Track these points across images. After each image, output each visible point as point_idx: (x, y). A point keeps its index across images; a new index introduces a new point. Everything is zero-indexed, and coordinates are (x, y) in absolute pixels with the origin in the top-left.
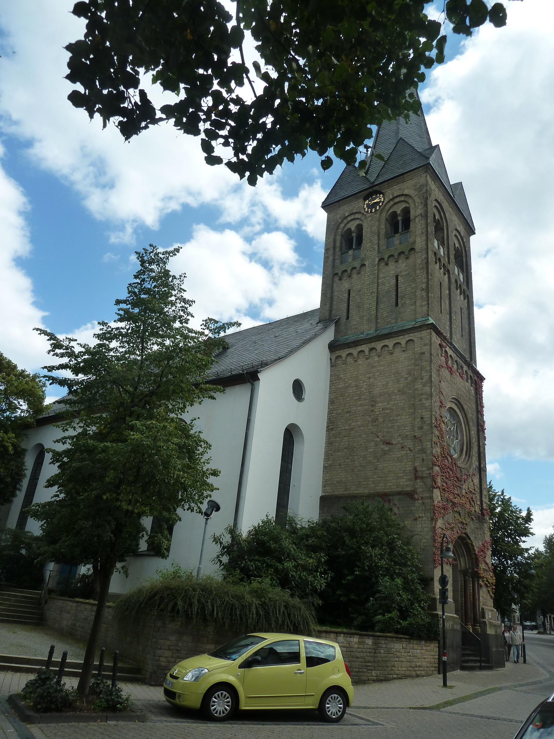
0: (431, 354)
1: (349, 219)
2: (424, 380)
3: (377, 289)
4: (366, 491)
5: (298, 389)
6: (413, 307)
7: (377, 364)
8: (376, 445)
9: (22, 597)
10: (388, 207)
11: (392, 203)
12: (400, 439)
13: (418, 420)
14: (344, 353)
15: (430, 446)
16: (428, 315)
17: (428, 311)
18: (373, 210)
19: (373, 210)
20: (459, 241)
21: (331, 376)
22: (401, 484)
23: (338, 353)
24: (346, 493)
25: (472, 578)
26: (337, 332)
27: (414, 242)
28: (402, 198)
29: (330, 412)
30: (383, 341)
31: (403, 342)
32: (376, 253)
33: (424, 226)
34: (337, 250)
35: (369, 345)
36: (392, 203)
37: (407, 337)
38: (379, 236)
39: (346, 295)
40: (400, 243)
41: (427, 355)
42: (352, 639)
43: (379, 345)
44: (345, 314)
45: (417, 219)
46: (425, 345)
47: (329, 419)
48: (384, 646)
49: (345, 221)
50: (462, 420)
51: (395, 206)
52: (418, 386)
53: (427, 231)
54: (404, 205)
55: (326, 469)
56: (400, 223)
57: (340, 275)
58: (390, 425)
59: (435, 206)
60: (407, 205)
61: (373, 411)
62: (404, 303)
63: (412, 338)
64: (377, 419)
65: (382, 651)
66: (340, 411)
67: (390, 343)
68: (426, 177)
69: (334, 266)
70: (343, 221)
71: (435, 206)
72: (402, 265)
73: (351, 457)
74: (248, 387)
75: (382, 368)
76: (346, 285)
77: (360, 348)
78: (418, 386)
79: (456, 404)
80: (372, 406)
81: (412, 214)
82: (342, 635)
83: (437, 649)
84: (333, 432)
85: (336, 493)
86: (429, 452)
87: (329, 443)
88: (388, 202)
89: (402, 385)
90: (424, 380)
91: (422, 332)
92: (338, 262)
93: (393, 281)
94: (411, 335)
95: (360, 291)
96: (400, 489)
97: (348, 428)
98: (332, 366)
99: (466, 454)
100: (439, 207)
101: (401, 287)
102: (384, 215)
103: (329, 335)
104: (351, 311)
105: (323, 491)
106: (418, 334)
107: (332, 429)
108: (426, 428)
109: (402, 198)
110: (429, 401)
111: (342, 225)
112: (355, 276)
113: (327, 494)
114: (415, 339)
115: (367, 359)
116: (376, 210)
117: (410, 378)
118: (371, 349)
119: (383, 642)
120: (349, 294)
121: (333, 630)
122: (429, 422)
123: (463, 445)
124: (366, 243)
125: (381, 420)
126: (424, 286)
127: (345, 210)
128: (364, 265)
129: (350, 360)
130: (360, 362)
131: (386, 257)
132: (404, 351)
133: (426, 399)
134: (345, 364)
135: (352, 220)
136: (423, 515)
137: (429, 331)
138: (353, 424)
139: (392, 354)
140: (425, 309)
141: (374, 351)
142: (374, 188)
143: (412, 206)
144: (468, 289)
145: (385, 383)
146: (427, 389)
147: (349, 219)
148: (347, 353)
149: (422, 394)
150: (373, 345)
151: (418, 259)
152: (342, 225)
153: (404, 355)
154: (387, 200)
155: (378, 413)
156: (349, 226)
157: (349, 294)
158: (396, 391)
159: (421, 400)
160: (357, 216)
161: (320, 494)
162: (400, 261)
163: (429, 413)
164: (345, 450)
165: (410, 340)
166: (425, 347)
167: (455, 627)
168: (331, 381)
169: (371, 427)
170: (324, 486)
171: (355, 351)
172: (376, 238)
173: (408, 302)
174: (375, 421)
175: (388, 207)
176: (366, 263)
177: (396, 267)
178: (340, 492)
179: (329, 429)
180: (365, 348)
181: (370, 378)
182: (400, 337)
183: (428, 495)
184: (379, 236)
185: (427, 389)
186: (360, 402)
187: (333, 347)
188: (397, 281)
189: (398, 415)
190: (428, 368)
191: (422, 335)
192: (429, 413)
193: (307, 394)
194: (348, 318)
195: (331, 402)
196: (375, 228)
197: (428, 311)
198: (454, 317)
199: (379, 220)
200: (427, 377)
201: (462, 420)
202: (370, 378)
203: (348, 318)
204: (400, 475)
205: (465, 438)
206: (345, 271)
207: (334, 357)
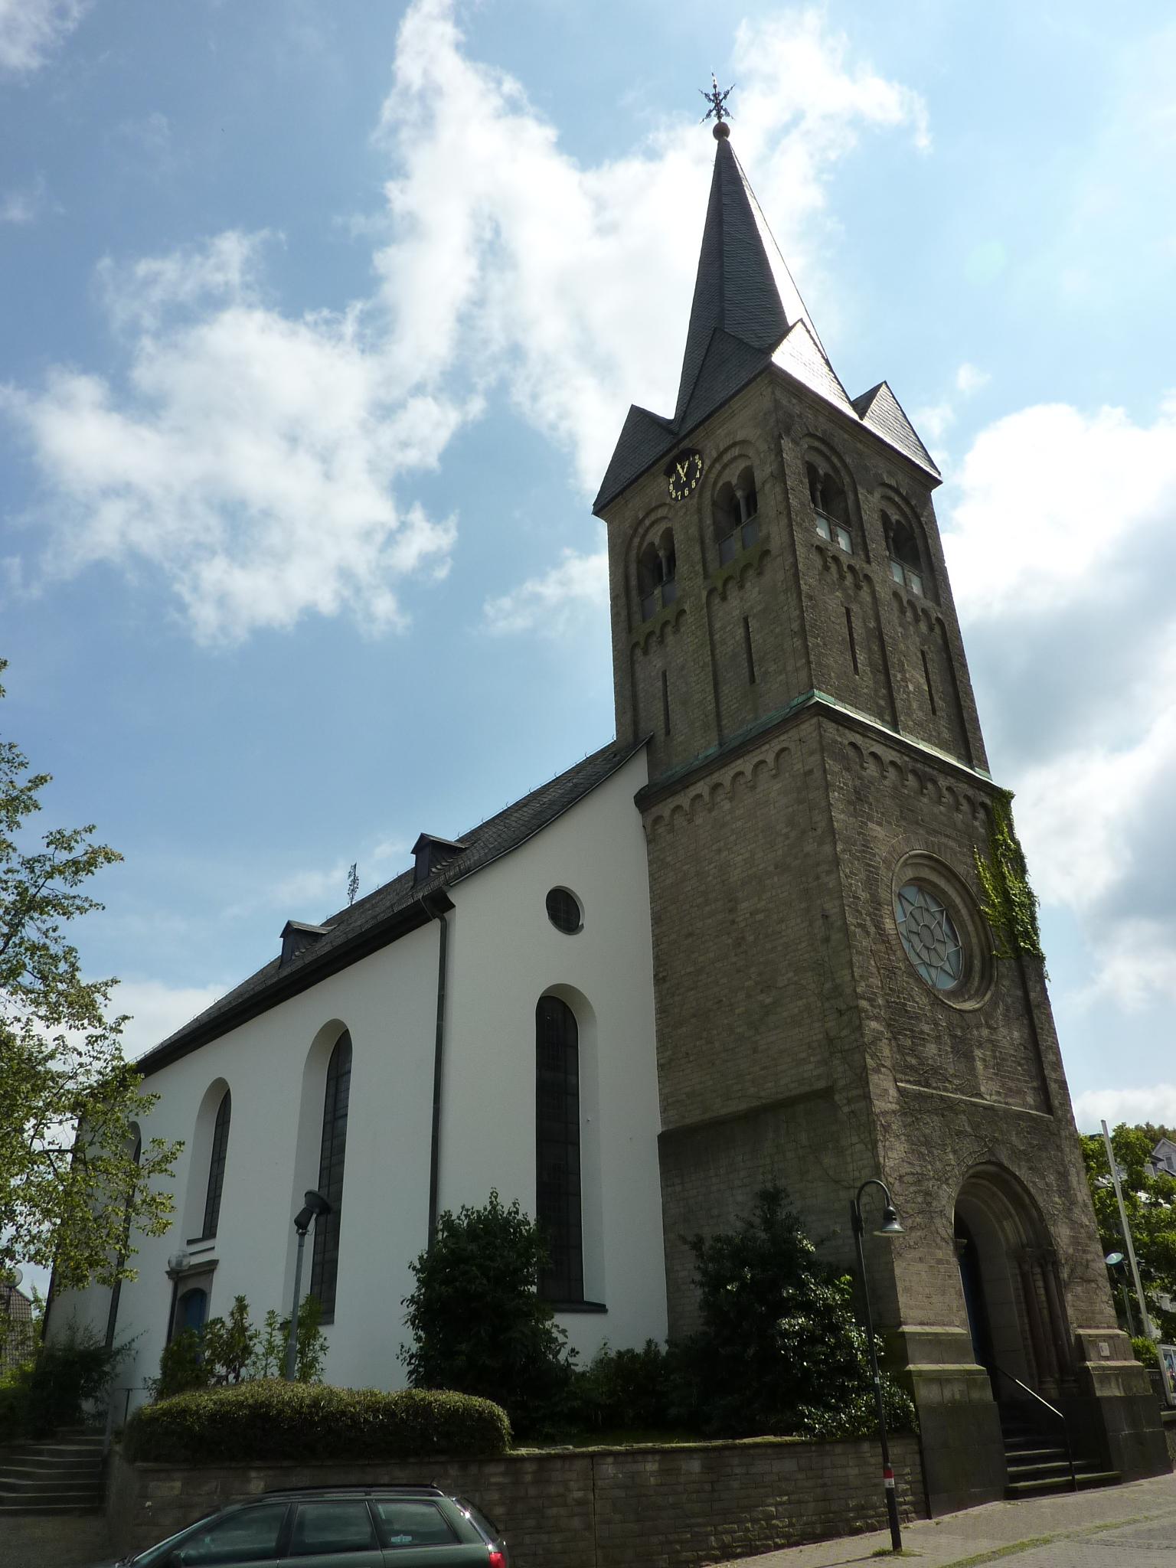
0: (825, 771)
1: (647, 522)
2: (819, 831)
3: (713, 655)
4: (743, 1106)
5: (564, 910)
6: (783, 677)
7: (728, 818)
8: (749, 996)
9: (78, 1453)
10: (713, 476)
11: (718, 467)
12: (791, 974)
13: (819, 923)
14: (665, 809)
15: (848, 978)
16: (812, 688)
17: (810, 677)
18: (686, 492)
19: (686, 492)
20: (898, 507)
21: (651, 863)
22: (806, 1075)
23: (655, 811)
24: (707, 1116)
25: (1041, 1266)
26: (652, 767)
27: (768, 538)
28: (736, 451)
29: (656, 944)
30: (733, 765)
31: (770, 758)
32: (700, 580)
33: (780, 498)
34: (634, 593)
35: (708, 779)
36: (718, 467)
37: (776, 745)
38: (702, 542)
39: (660, 684)
40: (744, 547)
41: (818, 774)
42: (640, 1467)
43: (725, 776)
44: (661, 724)
45: (768, 486)
46: (812, 754)
47: (656, 958)
48: (737, 1470)
49: (641, 531)
50: (958, 900)
51: (727, 471)
52: (810, 847)
53: (788, 506)
54: (742, 465)
55: (665, 1068)
56: (738, 506)
57: (642, 643)
58: (769, 946)
59: (811, 448)
60: (748, 463)
61: (733, 922)
62: (766, 673)
63: (784, 745)
64: (743, 938)
65: (736, 1485)
66: (674, 936)
67: (745, 765)
68: (773, 393)
69: (630, 630)
70: (636, 530)
71: (811, 448)
72: (753, 594)
73: (705, 1034)
74: (435, 926)
75: (739, 823)
76: (657, 663)
77: (693, 791)
78: (810, 847)
79: (934, 869)
80: (730, 911)
81: (759, 476)
82: (610, 1460)
83: (917, 1457)
84: (667, 985)
85: (688, 1121)
86: (848, 991)
87: (662, 1011)
88: (711, 467)
89: (780, 852)
90: (819, 831)
91: (803, 727)
92: (637, 617)
93: (740, 632)
94: (782, 738)
95: (683, 668)
96: (806, 1089)
97: (692, 969)
98: (649, 842)
99: (982, 977)
100: (823, 447)
101: (756, 638)
102: (708, 495)
103: (637, 776)
104: (672, 715)
105: (664, 1122)
106: (793, 734)
107: (664, 978)
108: (836, 936)
109: (736, 451)
110: (834, 876)
111: (637, 540)
112: (670, 639)
113: (671, 1127)
114: (792, 746)
115: (710, 811)
116: (691, 491)
117: (793, 834)
118: (717, 786)
119: (736, 1461)
120: (665, 681)
121: (658, 1445)
122: (839, 923)
123: (971, 957)
124: (682, 568)
125: (751, 938)
126: (795, 626)
127: (635, 506)
128: (684, 611)
129: (680, 821)
130: (699, 821)
131: (719, 585)
132: (775, 776)
133: (829, 873)
134: (672, 830)
135: (653, 524)
136: (855, 1139)
137: (814, 720)
138: (701, 959)
139: (753, 788)
140: (803, 675)
141: (720, 791)
142: (682, 446)
143: (757, 462)
144: (939, 604)
145: (747, 855)
146: (827, 849)
147: (647, 522)
148: (672, 806)
149: (818, 865)
150: (716, 777)
151: (776, 572)
152: (637, 540)
153: (777, 786)
154: (708, 462)
155: (742, 924)
156: (649, 538)
157: (665, 681)
158: (771, 868)
159: (818, 878)
160: (661, 513)
161: (659, 1129)
162: (748, 585)
163: (837, 903)
164: (693, 1020)
165: (783, 750)
166: (813, 758)
167: (975, 1395)
168: (651, 875)
169: (734, 959)
170: (664, 1110)
171: (684, 800)
172: (697, 549)
173: (772, 668)
174: (739, 945)
175: (713, 476)
176: (686, 607)
177: (742, 599)
178: (694, 1116)
179: (659, 980)
180: (702, 788)
181: (719, 851)
182: (764, 748)
183: (859, 1092)
184: (702, 542)
185: (827, 849)
186: (707, 909)
187: (644, 800)
188: (747, 627)
189: (781, 921)
190: (823, 804)
191: (803, 734)
192: (837, 903)
193: (588, 917)
194: (668, 732)
195: (657, 919)
196: (693, 531)
197: (810, 677)
198: (899, 676)
199: (699, 511)
200: (823, 824)
201: (958, 900)
202: (719, 851)
203: (668, 732)
204: (803, 1055)
205: (974, 940)
206: (651, 634)
207: (649, 821)
